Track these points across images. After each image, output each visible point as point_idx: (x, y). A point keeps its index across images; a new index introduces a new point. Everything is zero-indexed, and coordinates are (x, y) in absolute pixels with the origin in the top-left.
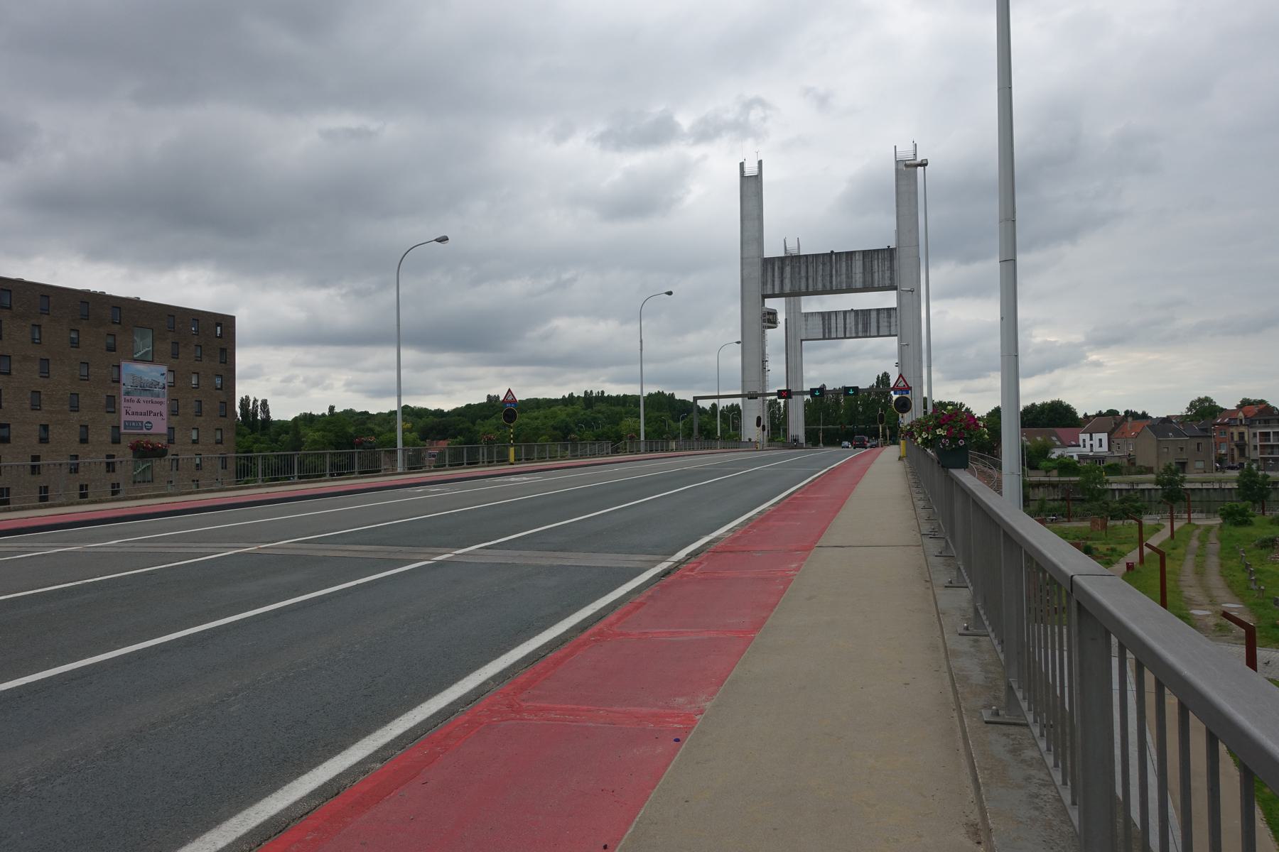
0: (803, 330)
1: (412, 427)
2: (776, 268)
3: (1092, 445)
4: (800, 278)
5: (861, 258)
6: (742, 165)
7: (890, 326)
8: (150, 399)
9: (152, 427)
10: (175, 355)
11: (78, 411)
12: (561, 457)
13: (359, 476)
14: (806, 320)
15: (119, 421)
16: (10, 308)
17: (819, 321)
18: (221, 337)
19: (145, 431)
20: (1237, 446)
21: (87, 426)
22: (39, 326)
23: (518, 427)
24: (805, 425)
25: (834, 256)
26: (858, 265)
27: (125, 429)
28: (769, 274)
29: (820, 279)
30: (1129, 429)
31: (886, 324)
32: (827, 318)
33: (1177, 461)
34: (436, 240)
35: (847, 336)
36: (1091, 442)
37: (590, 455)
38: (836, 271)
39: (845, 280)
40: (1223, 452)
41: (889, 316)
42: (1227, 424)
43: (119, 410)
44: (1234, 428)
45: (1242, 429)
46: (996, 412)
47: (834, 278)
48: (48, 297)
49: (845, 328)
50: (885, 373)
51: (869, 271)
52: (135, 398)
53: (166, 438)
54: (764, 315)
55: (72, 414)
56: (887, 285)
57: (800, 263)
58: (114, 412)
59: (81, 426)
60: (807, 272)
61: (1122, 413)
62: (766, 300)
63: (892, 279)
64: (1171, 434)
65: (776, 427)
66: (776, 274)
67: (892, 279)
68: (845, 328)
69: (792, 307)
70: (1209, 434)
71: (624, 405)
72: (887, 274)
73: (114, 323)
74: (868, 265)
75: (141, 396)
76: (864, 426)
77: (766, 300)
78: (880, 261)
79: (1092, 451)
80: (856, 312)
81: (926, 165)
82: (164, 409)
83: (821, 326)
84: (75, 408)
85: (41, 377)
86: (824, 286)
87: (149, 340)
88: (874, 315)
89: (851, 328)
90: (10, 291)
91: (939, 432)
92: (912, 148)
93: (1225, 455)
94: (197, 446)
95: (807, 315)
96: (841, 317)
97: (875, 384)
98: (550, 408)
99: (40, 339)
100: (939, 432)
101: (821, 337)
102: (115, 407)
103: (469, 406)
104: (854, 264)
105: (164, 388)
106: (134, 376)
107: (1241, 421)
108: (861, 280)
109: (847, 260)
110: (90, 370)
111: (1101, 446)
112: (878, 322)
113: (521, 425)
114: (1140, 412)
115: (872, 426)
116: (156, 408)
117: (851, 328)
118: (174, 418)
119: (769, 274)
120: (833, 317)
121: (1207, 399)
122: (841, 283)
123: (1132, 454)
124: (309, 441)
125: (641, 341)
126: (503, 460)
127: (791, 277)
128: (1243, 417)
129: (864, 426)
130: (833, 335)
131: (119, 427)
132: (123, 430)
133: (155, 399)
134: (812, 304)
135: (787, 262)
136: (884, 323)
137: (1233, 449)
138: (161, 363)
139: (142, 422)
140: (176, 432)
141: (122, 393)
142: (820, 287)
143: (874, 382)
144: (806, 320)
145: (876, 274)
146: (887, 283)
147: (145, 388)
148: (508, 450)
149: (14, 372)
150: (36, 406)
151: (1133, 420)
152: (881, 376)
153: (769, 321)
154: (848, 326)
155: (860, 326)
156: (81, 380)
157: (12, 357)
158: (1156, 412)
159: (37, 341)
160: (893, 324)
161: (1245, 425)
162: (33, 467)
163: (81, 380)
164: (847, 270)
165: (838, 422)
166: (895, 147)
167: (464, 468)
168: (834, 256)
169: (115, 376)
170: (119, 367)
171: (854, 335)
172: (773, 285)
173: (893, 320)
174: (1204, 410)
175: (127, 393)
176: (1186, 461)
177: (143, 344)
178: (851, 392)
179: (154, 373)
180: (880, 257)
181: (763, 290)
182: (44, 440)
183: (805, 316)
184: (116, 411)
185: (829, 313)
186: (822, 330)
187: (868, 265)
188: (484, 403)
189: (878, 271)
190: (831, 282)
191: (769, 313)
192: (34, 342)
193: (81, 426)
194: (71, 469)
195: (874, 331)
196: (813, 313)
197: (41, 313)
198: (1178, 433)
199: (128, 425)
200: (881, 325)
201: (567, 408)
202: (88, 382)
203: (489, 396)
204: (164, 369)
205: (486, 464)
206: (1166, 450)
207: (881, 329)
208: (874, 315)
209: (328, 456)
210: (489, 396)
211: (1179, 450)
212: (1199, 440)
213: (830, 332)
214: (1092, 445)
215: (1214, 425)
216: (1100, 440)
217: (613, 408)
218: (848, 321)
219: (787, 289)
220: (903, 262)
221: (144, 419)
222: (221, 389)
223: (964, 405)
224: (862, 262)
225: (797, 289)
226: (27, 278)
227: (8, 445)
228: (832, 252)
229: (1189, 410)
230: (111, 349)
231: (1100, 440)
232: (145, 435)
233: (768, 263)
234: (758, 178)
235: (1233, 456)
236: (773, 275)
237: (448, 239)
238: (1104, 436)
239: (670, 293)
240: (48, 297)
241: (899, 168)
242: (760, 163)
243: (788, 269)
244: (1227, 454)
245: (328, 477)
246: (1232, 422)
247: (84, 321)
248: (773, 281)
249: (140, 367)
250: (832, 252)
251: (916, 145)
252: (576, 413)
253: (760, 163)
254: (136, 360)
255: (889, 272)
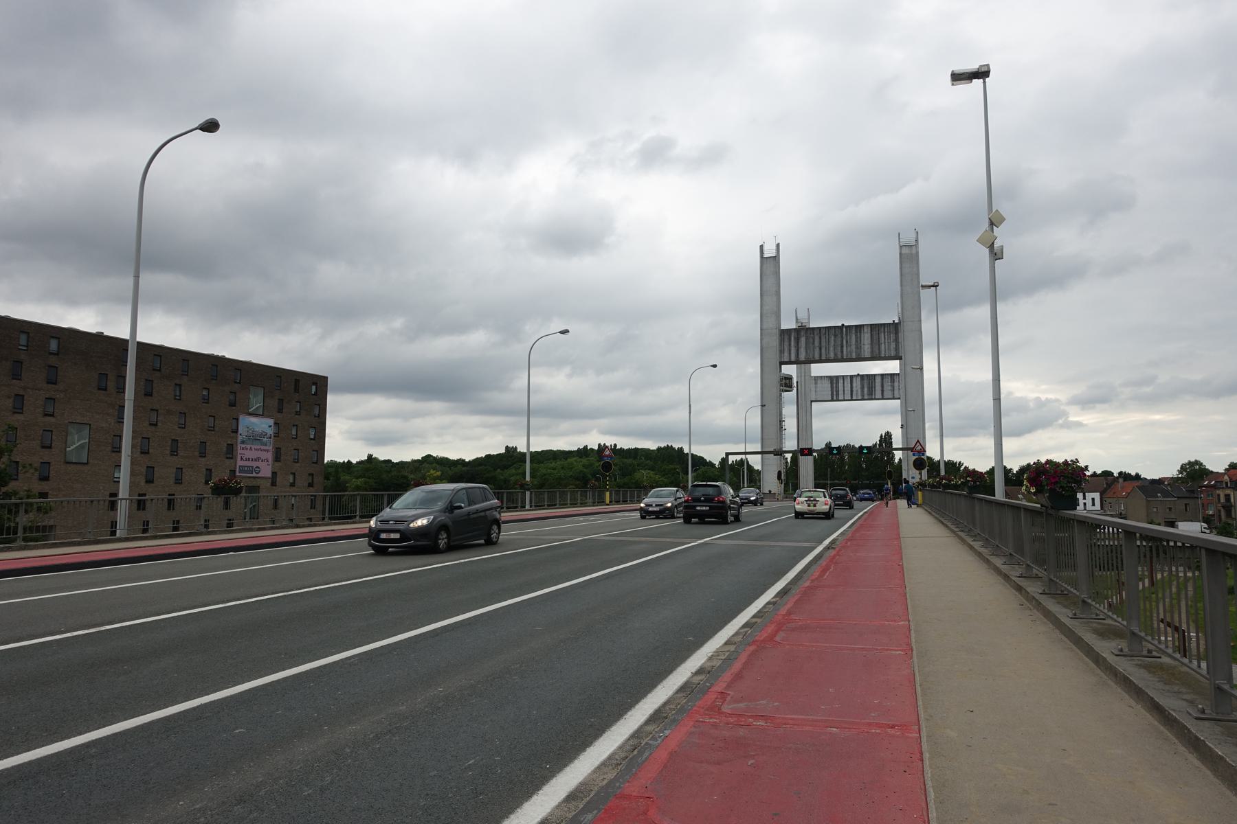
0: (813, 393)
1: (441, 475)
2: (792, 338)
3: (1085, 504)
4: (814, 348)
5: (869, 331)
6: (761, 247)
7: (894, 390)
8: (259, 447)
9: (260, 471)
10: (280, 410)
11: (205, 456)
12: (581, 504)
13: (330, 521)
14: (816, 383)
15: (235, 465)
16: (160, 370)
17: (827, 384)
18: (316, 394)
19: (254, 475)
20: (1223, 507)
21: (210, 470)
22: (180, 385)
23: (543, 476)
24: (815, 480)
25: (844, 329)
26: (866, 337)
27: (239, 473)
28: (786, 343)
29: (832, 349)
30: (1120, 489)
31: (890, 388)
32: (835, 381)
33: (1166, 520)
34: (560, 332)
35: (854, 398)
36: (1085, 501)
37: (548, 505)
38: (847, 342)
39: (854, 350)
40: (1211, 513)
41: (893, 381)
42: (1214, 487)
43: (236, 458)
44: (1221, 490)
45: (1228, 491)
46: (992, 470)
47: (845, 348)
48: (188, 361)
49: (852, 391)
50: (888, 432)
51: (875, 342)
52: (248, 446)
53: (270, 481)
54: (781, 380)
55: (201, 459)
56: (892, 355)
57: (814, 334)
58: (232, 458)
59: (207, 469)
60: (820, 342)
61: (1116, 475)
62: (783, 366)
63: (897, 349)
64: (1159, 495)
65: (790, 479)
66: (793, 344)
67: (897, 349)
68: (852, 391)
69: (803, 370)
70: (1196, 496)
71: (635, 458)
72: (893, 345)
73: (236, 382)
74: (875, 337)
75: (253, 444)
76: (868, 482)
77: (783, 366)
78: (886, 333)
79: (1085, 509)
80: (862, 377)
81: (937, 286)
82: (270, 456)
83: (830, 389)
84: (203, 454)
85: (179, 428)
86: (836, 355)
87: (261, 397)
88: (878, 380)
89: (857, 391)
90: (161, 356)
91: (968, 479)
92: (913, 235)
93: (1213, 516)
94: (294, 488)
95: (816, 378)
96: (848, 381)
97: (878, 443)
98: (566, 459)
99: (180, 396)
100: (968, 479)
101: (830, 399)
102: (232, 454)
103: (488, 456)
104: (862, 336)
105: (270, 438)
106: (248, 427)
107: (1227, 483)
108: (869, 350)
109: (856, 332)
110: (216, 422)
111: (1093, 505)
112: (882, 386)
113: (545, 475)
114: (1133, 474)
115: (876, 482)
116: (264, 455)
117: (857, 391)
118: (277, 464)
119: (786, 343)
120: (841, 381)
121: (1197, 462)
122: (851, 352)
123: (1123, 512)
124: (353, 486)
125: (690, 406)
126: (602, 502)
127: (806, 347)
128: (1229, 480)
129: (868, 482)
130: (841, 397)
131: (235, 471)
132: (238, 474)
133: (263, 448)
134: (818, 369)
135: (802, 333)
136: (887, 387)
137: (1220, 511)
138: (269, 417)
139: (252, 467)
140: (278, 476)
141: (239, 441)
142: (832, 356)
143: (877, 440)
144: (816, 383)
145: (883, 345)
146: (893, 353)
147: (256, 438)
148: (604, 495)
149: (159, 424)
150: (174, 452)
151: (1124, 481)
152: (883, 435)
153: (786, 385)
154: (854, 389)
155: (866, 390)
156: (209, 430)
157: (159, 411)
158: (1149, 474)
159: (177, 398)
160: (896, 388)
161: (1230, 488)
162: (139, 501)
163: (209, 430)
164: (856, 341)
165: (843, 477)
166: (899, 234)
167: (628, 504)
168: (844, 329)
169: (234, 427)
170: (237, 419)
171: (860, 398)
172: (790, 354)
173: (896, 384)
174: (1194, 473)
175: (243, 442)
176: (1174, 520)
177: (257, 402)
178: (865, 451)
179: (263, 425)
180: (886, 330)
181: (780, 357)
182: (178, 481)
183: (815, 380)
184: (234, 457)
185: (837, 377)
186: (830, 393)
187: (875, 337)
188: (503, 454)
189: (885, 342)
190: (842, 352)
191: (786, 378)
192: (175, 399)
193: (207, 469)
194: (197, 506)
195: (878, 395)
196: (821, 377)
197: (182, 375)
198: (1166, 494)
199: (242, 469)
200: (885, 389)
201: (582, 460)
202: (213, 432)
203: (507, 447)
204: (271, 422)
205: (533, 508)
206: (1155, 510)
207: (885, 393)
208: (878, 380)
209: (558, 493)
210: (507, 447)
211: (1168, 510)
212: (1186, 501)
213: (838, 395)
214: (1085, 504)
215: (1201, 487)
216: (1093, 499)
217: (626, 460)
218: (854, 385)
219: (802, 357)
220: (907, 335)
221: (254, 464)
222: (314, 439)
223: (963, 464)
224: (869, 334)
225: (811, 357)
226: (13, 316)
227: (152, 485)
228: (843, 325)
229: (1180, 472)
230: (232, 405)
231: (1093, 499)
232: (254, 478)
233: (785, 333)
234: (776, 259)
235: (1220, 516)
236: (790, 345)
237: (568, 332)
238: (1097, 496)
239: (715, 366)
240: (188, 361)
241: (903, 252)
242: (778, 245)
243: (803, 340)
244: (1214, 515)
245: (20, 543)
246: (1219, 484)
247: (214, 381)
248: (790, 350)
249: (254, 420)
250: (843, 325)
251: (917, 233)
252: (591, 465)
253: (778, 245)
254: (251, 414)
255: (894, 343)
